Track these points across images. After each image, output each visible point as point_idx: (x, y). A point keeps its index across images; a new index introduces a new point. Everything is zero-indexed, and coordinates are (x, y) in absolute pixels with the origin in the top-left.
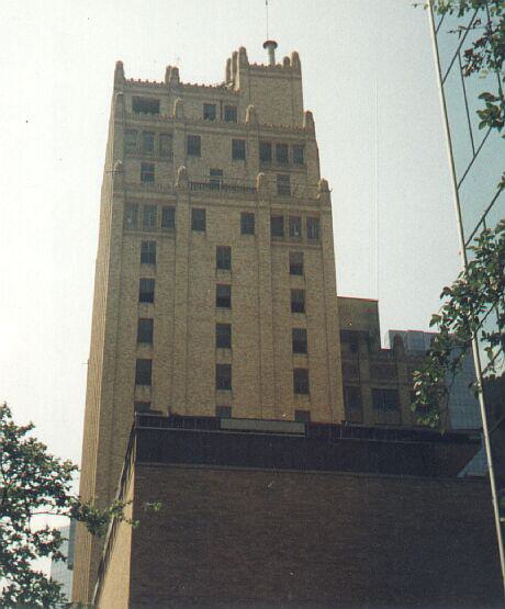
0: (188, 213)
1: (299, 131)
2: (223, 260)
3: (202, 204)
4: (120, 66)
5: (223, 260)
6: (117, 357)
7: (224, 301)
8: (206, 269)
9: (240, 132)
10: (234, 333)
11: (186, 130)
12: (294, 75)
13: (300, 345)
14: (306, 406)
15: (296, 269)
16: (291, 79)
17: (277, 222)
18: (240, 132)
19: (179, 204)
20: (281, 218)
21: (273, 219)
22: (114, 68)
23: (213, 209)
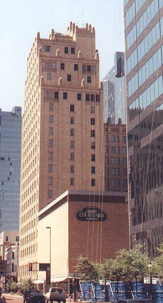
0: (62, 94)
1: (93, 60)
2: (72, 108)
3: (66, 90)
4: (39, 34)
5: (72, 108)
6: (44, 139)
7: (72, 122)
8: (67, 111)
9: (76, 61)
10: (72, 77)
11: (63, 90)
12: (93, 36)
13: (93, 134)
14: (95, 177)
15: (93, 111)
16: (92, 37)
17: (87, 96)
18: (76, 61)
19: (60, 91)
20: (89, 95)
21: (86, 95)
22: (37, 34)
23: (70, 92)
